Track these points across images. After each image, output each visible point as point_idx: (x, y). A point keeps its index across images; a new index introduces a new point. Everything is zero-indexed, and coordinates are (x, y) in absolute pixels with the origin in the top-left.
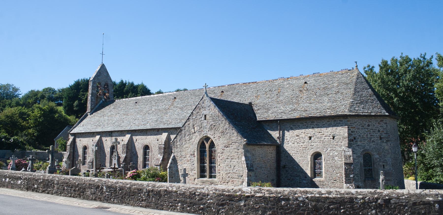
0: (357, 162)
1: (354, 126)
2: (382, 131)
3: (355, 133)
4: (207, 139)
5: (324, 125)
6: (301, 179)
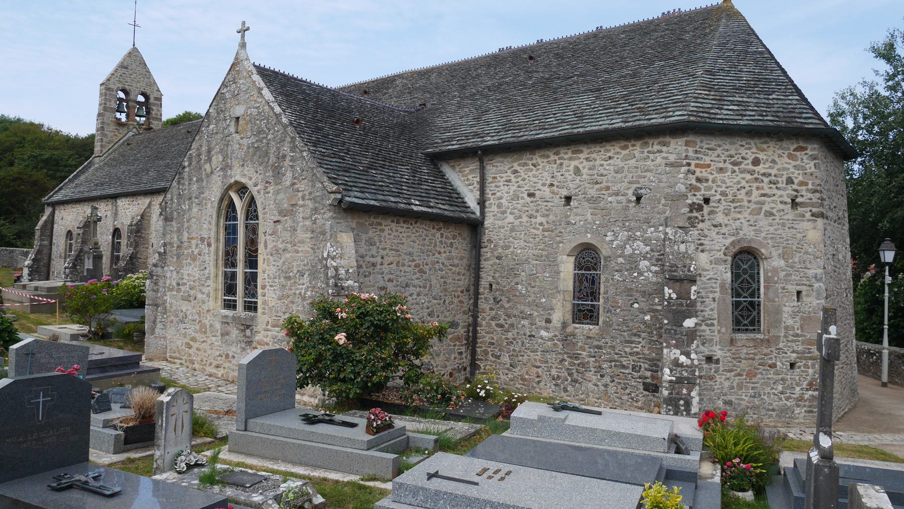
0: (709, 279)
1: (708, 162)
2: (802, 184)
3: (710, 183)
4: (242, 189)
5: (610, 158)
6: (534, 327)
